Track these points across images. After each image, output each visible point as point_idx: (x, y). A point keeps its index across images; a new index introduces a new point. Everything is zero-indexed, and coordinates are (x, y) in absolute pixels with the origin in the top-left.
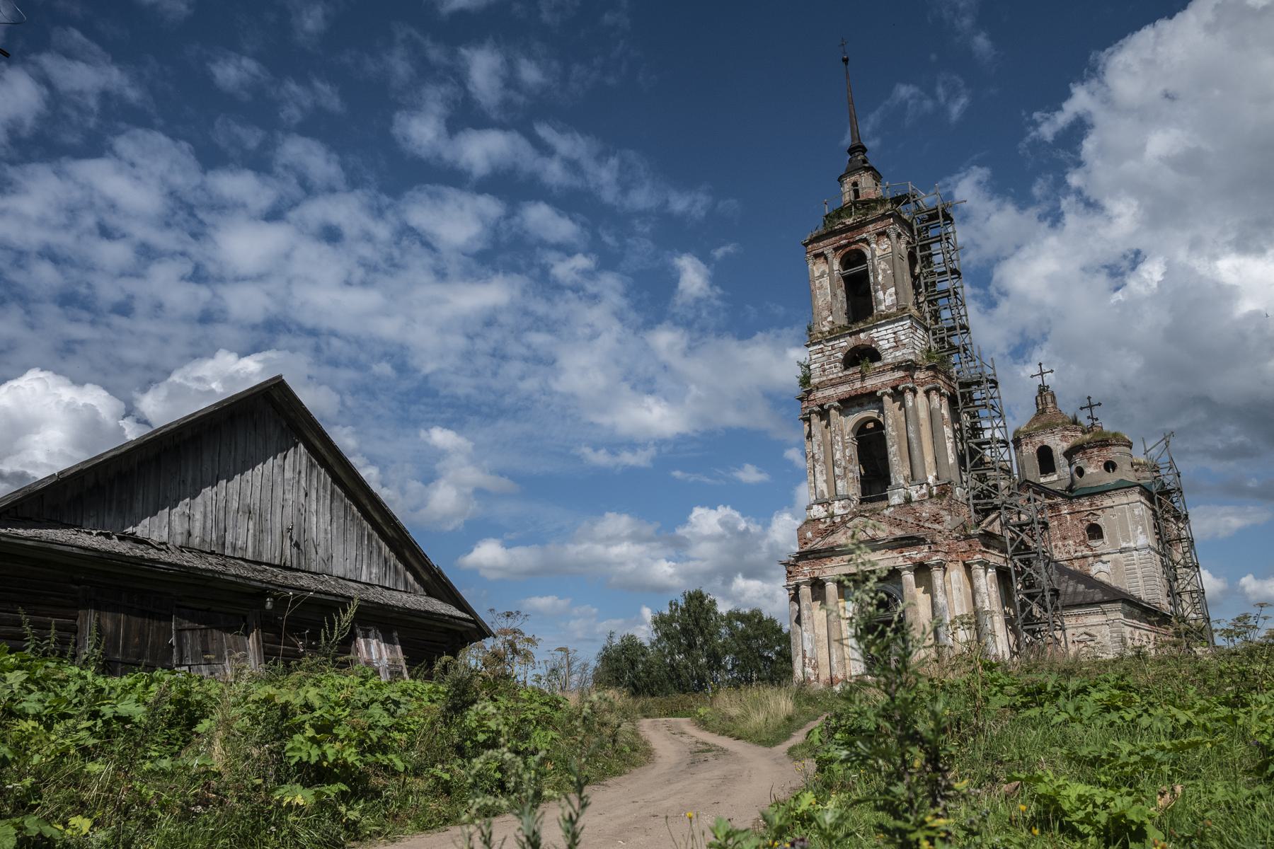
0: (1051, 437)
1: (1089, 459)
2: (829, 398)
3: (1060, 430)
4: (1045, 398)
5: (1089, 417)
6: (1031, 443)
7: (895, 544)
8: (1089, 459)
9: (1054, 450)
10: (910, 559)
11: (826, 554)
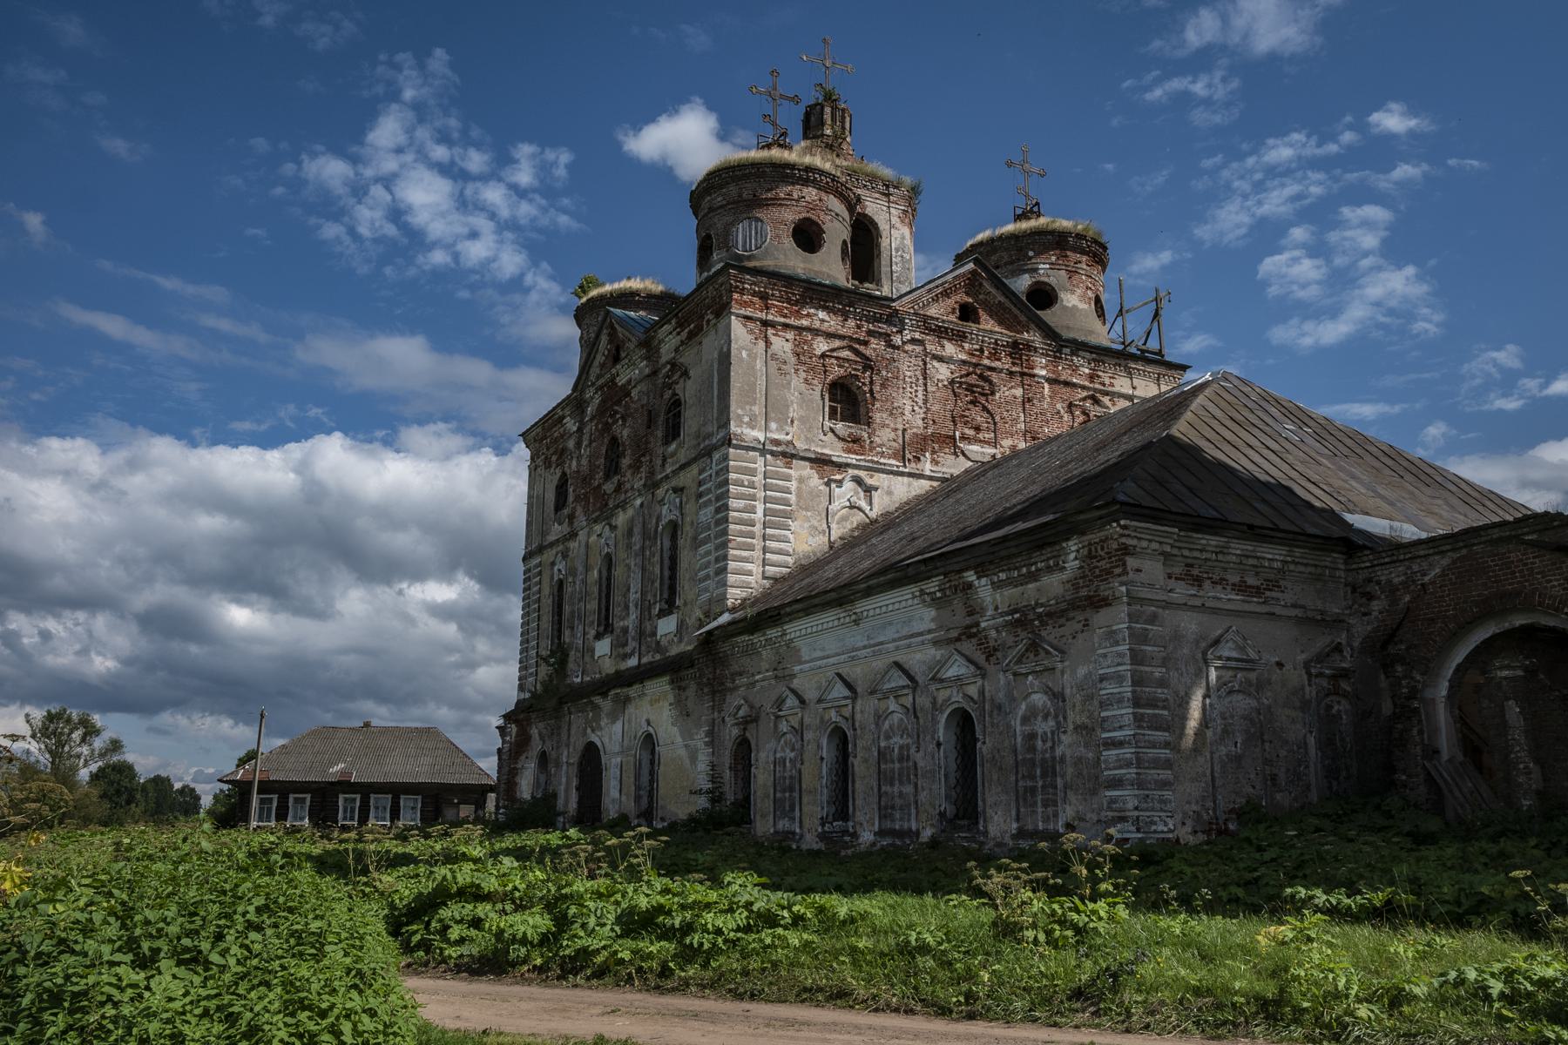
9: (885, 234)
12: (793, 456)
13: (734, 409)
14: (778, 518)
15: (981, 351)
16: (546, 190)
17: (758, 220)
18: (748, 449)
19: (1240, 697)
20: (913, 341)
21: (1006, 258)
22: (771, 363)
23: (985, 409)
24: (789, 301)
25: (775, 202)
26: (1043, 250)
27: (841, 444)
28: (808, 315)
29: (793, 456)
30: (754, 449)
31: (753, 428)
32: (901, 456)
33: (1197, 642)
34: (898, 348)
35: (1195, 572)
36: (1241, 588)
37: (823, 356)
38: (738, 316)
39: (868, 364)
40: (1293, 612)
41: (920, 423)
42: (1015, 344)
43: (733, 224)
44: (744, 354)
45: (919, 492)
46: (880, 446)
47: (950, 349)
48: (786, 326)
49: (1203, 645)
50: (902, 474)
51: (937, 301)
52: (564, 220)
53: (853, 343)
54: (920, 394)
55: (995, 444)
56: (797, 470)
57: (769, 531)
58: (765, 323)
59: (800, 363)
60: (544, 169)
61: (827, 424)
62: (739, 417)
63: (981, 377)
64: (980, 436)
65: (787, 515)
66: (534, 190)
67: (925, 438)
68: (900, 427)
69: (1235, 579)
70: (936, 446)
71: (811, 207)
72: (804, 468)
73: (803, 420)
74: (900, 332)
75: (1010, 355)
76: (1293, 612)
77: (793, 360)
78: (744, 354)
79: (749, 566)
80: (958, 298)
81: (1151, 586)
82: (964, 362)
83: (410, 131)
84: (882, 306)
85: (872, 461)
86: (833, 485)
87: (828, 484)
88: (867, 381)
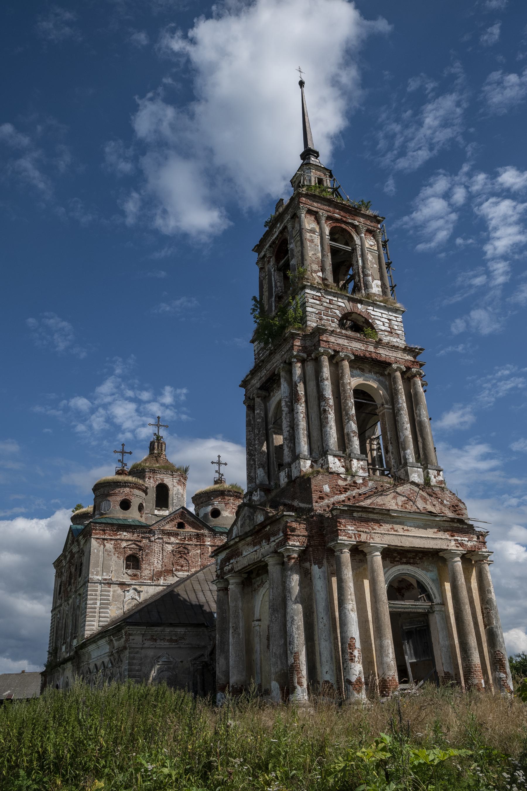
0: (171, 478)
1: (226, 504)
2: (343, 347)
3: (179, 475)
4: (162, 446)
5: (216, 471)
6: (153, 478)
7: (447, 524)
8: (226, 504)
9: (171, 489)
10: (462, 545)
11: (375, 516)
12: (111, 584)
13: (91, 570)
14: (105, 605)
15: (185, 538)
16: (177, 406)
17: (109, 501)
18: (95, 583)
19: (166, 672)
20: (159, 538)
21: (205, 500)
22: (105, 552)
23: (185, 559)
24: (113, 531)
25: (115, 494)
26: (216, 496)
27: (130, 577)
28: (120, 534)
29: (111, 584)
30: (97, 583)
31: (97, 576)
32: (152, 579)
33: (153, 658)
34: (152, 542)
35: (155, 637)
36: (171, 641)
37: (124, 548)
38: (94, 538)
39: (141, 549)
40: (188, 646)
41: (160, 566)
42: (198, 535)
43: (101, 502)
44: (95, 551)
45: (158, 591)
46: (144, 576)
47: (173, 539)
48: (111, 539)
49: (155, 658)
50: (152, 585)
51: (169, 523)
52: (184, 417)
53: (135, 542)
54: (161, 557)
55: (188, 571)
56: (113, 588)
57: (101, 610)
58: (104, 539)
59: (116, 551)
60: (176, 397)
61: (125, 571)
62: (93, 572)
63: (184, 548)
64: (183, 569)
65: (108, 604)
66: (172, 405)
67: (161, 572)
68: (152, 569)
69: (169, 638)
70: (166, 574)
71: (127, 495)
72: (116, 587)
73: (116, 571)
74: (154, 536)
75: (196, 538)
76: (188, 646)
77: (113, 550)
78: (95, 551)
79: (93, 623)
80: (177, 521)
81: (137, 643)
82: (178, 543)
83: (118, 387)
84: (146, 528)
85: (141, 582)
86: (126, 592)
87: (124, 592)
88: (141, 554)
